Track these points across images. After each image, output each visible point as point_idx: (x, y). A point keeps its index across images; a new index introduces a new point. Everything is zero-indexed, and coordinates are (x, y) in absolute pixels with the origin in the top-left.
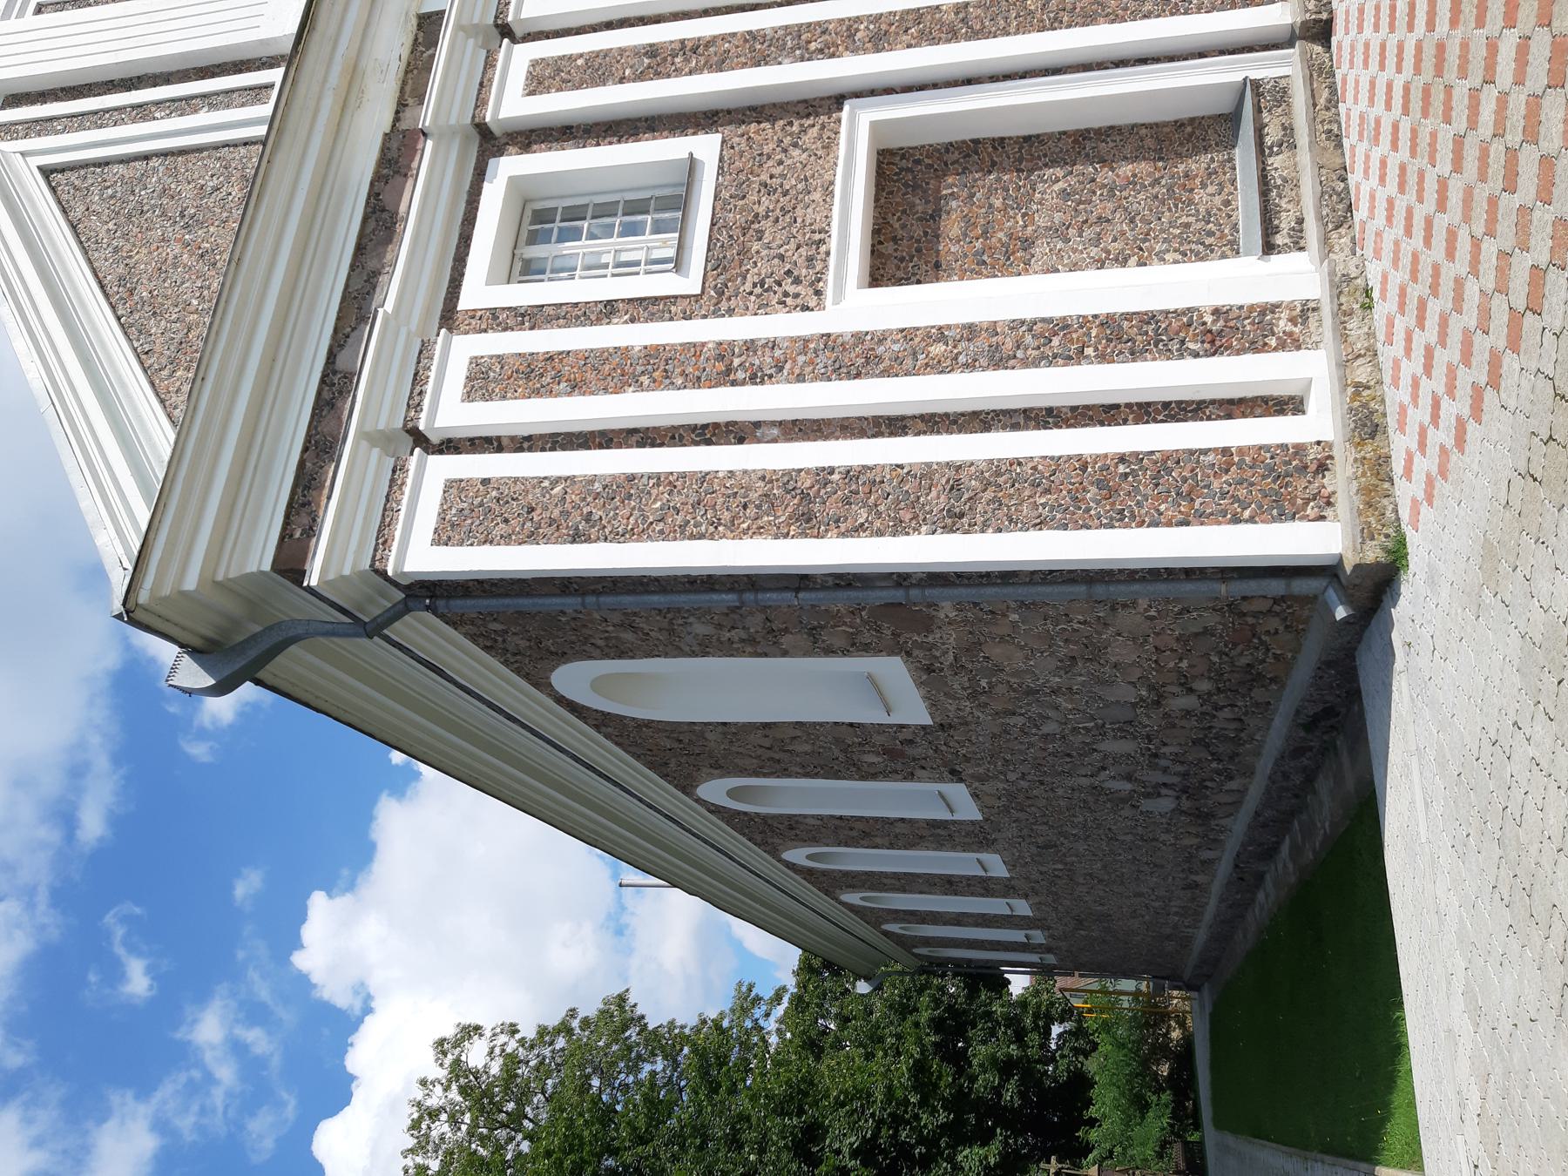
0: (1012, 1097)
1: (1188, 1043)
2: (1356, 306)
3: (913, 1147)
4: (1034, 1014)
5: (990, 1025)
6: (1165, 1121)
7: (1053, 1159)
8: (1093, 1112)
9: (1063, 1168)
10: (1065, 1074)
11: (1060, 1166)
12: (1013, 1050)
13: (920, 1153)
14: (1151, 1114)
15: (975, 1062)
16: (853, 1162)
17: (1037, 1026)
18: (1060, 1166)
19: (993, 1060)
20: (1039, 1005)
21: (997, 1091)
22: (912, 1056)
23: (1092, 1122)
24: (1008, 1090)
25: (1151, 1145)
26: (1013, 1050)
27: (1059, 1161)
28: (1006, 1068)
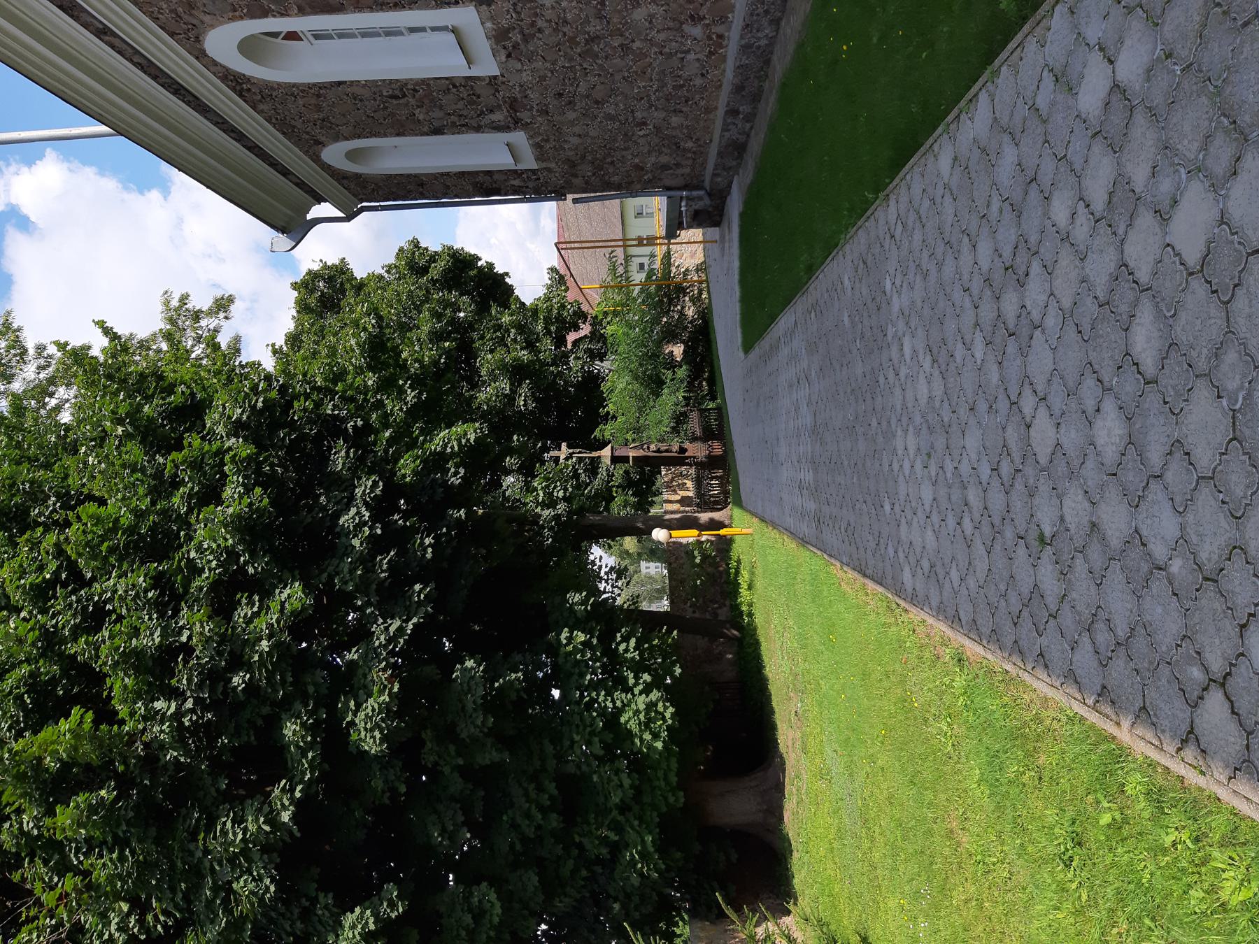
0: (525, 400)
1: (705, 317)
2: (687, 299)
3: (344, 420)
4: (545, 319)
5: (498, 334)
6: (681, 395)
7: (564, 445)
8: (611, 408)
9: (574, 453)
10: (579, 374)
11: (571, 451)
12: (524, 355)
13: (355, 427)
14: (666, 391)
15: (483, 372)
16: (233, 440)
17: (549, 332)
18: (571, 451)
19: (503, 366)
20: (550, 311)
21: (511, 398)
22: (365, 329)
23: (606, 418)
24: (520, 395)
25: (666, 422)
26: (524, 355)
27: (569, 447)
28: (518, 372)
